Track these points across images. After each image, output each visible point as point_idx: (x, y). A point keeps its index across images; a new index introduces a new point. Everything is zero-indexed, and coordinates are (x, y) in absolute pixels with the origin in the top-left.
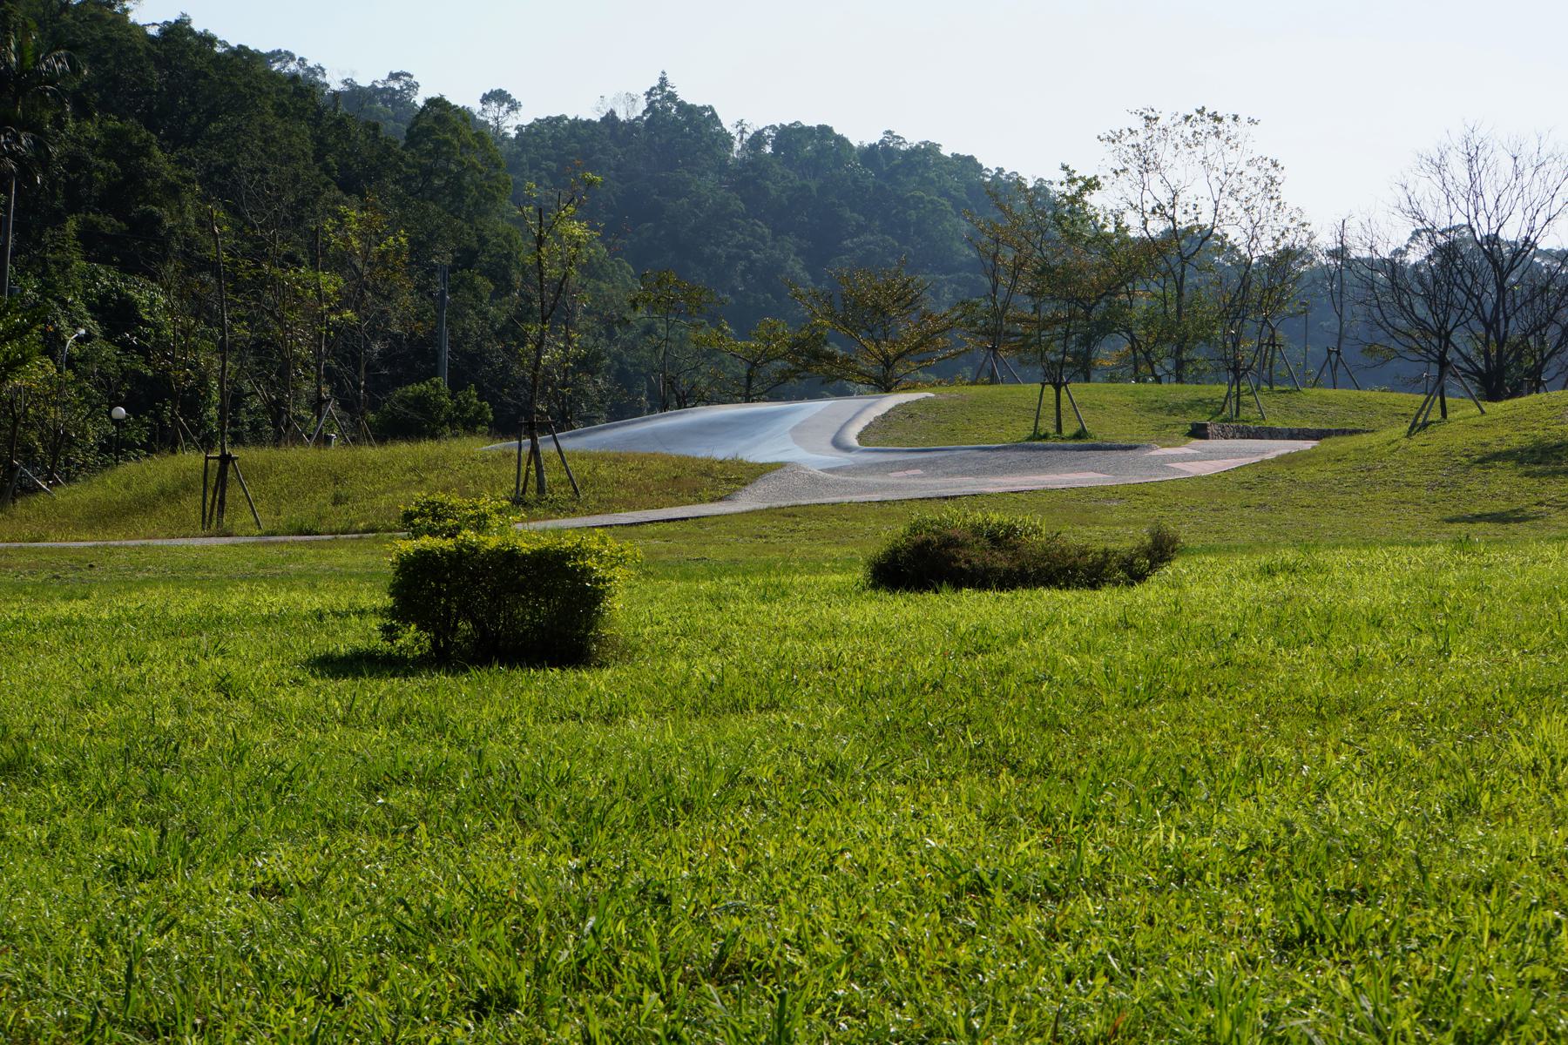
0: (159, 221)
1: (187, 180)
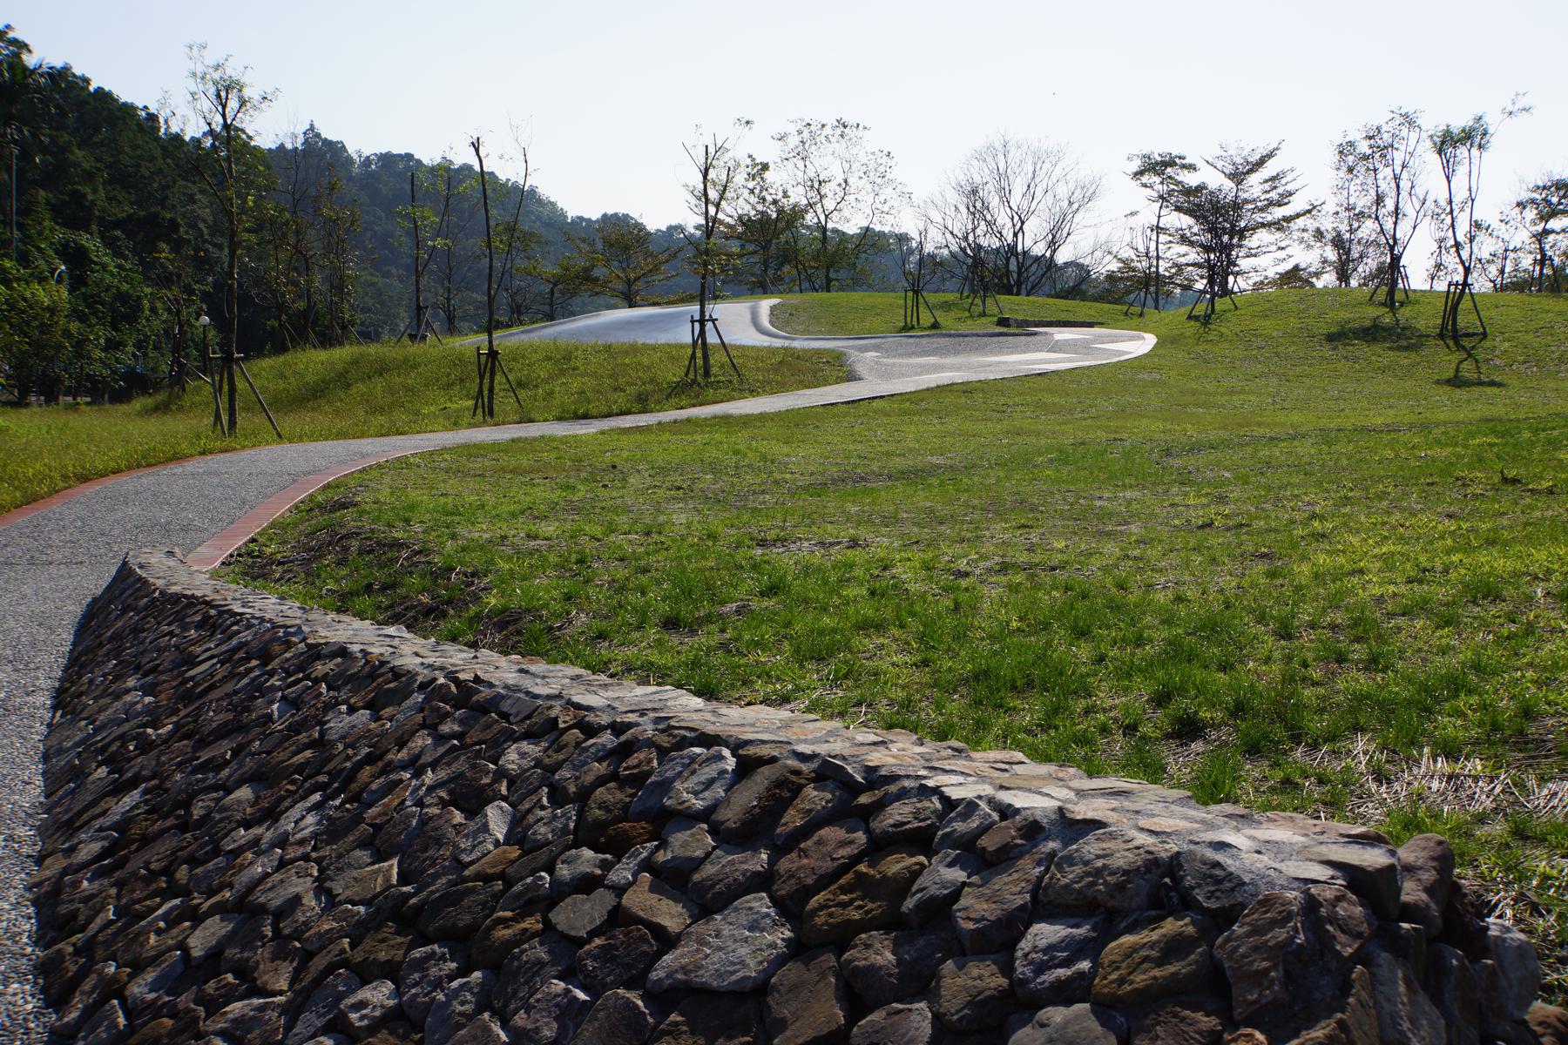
0: (84, 196)
1: (98, 169)
